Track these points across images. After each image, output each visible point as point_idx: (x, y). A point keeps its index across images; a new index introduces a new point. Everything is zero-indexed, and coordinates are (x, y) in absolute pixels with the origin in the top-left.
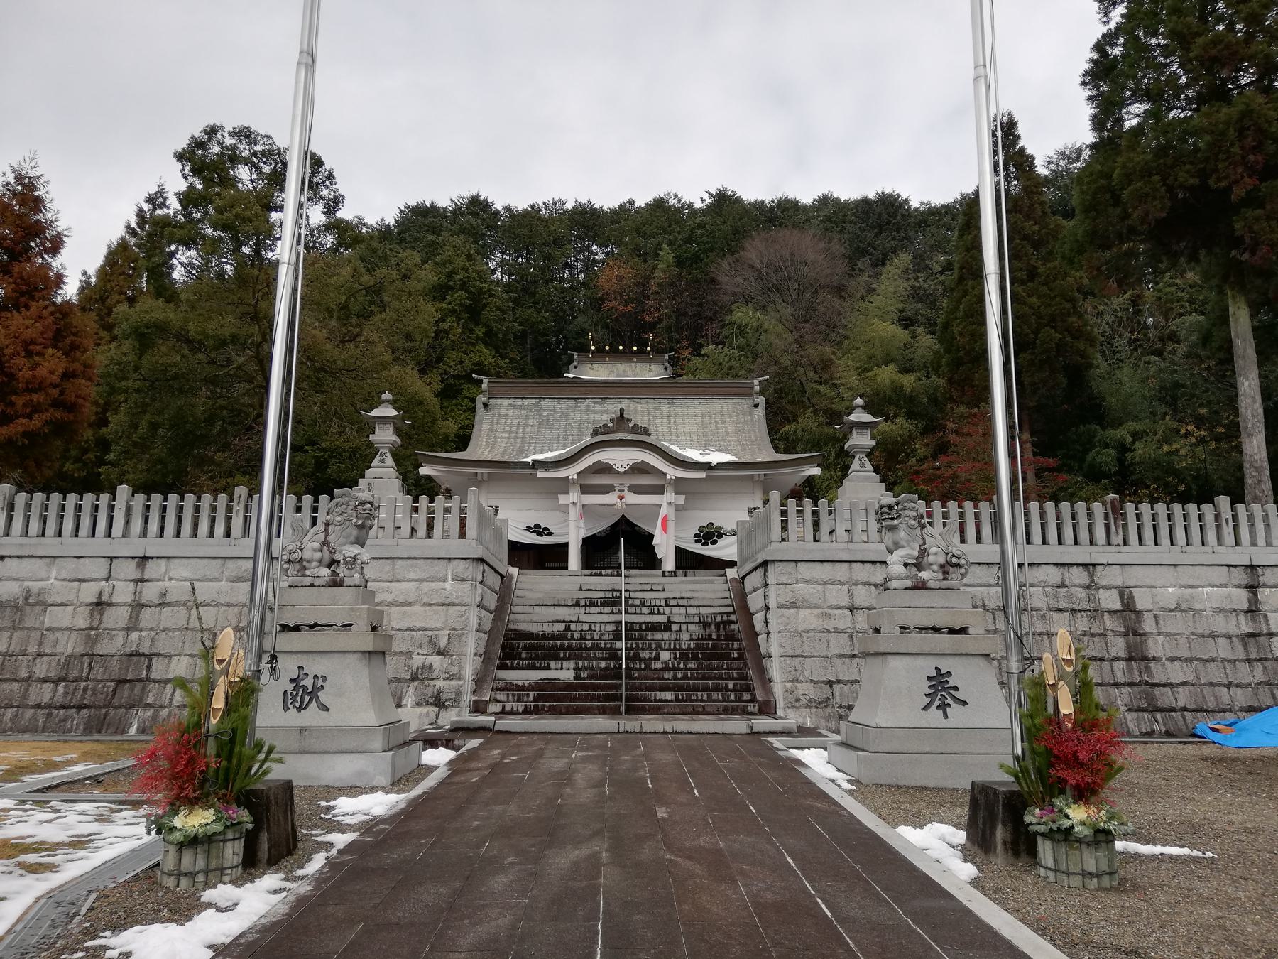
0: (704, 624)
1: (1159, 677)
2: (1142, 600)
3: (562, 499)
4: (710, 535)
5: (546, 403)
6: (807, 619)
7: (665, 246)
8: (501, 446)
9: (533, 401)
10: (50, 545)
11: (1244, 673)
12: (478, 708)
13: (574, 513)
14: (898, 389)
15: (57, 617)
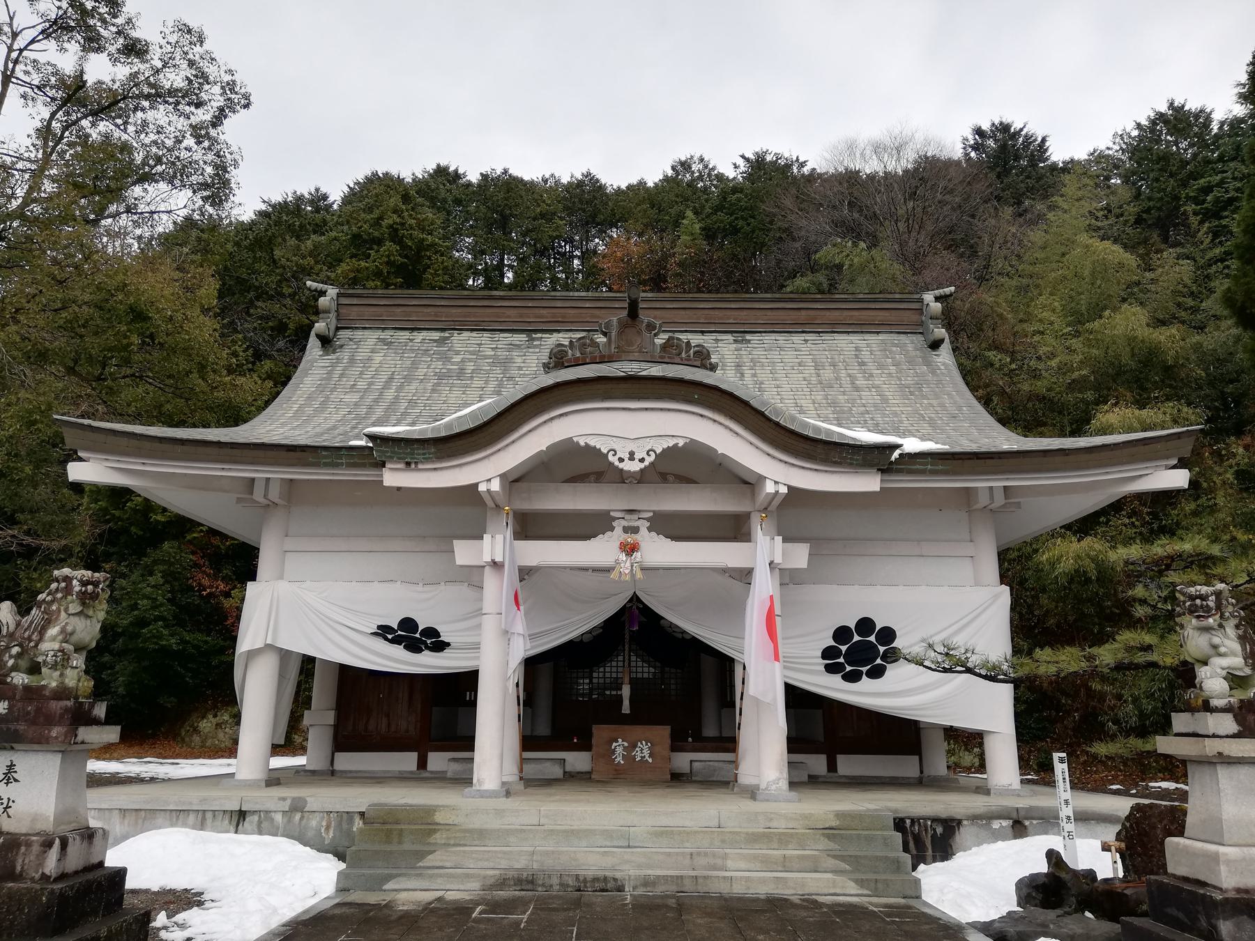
3: (464, 553)
4: (862, 649)
5: (463, 341)
7: (689, 213)
9: (436, 335)
13: (496, 591)
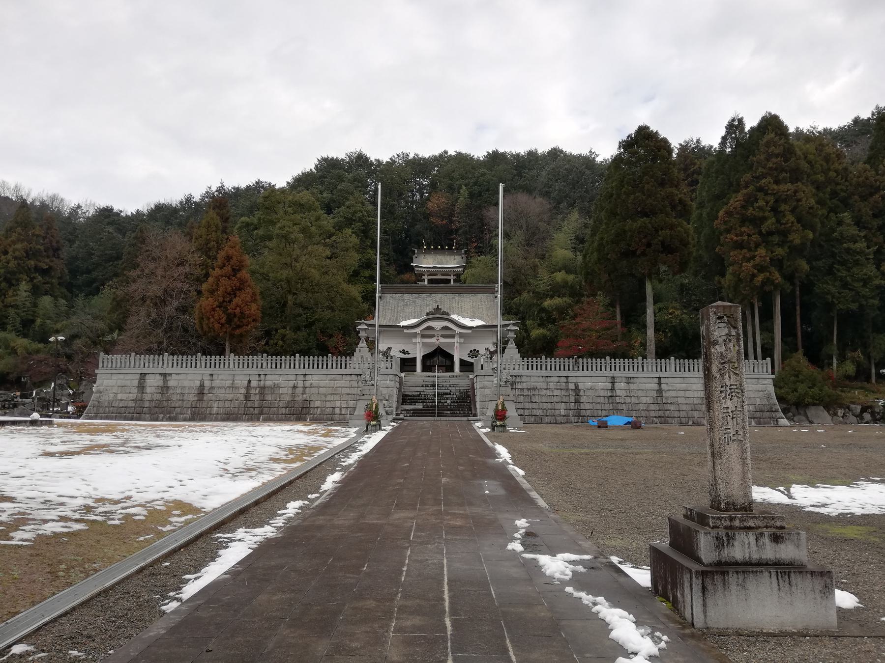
0: (461, 393)
1: (582, 407)
2: (581, 386)
3: (414, 340)
5: (406, 296)
6: (487, 392)
7: (464, 187)
8: (389, 317)
10: (278, 371)
11: (607, 407)
12: (397, 415)
14: (565, 284)
15: (282, 391)
